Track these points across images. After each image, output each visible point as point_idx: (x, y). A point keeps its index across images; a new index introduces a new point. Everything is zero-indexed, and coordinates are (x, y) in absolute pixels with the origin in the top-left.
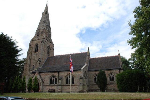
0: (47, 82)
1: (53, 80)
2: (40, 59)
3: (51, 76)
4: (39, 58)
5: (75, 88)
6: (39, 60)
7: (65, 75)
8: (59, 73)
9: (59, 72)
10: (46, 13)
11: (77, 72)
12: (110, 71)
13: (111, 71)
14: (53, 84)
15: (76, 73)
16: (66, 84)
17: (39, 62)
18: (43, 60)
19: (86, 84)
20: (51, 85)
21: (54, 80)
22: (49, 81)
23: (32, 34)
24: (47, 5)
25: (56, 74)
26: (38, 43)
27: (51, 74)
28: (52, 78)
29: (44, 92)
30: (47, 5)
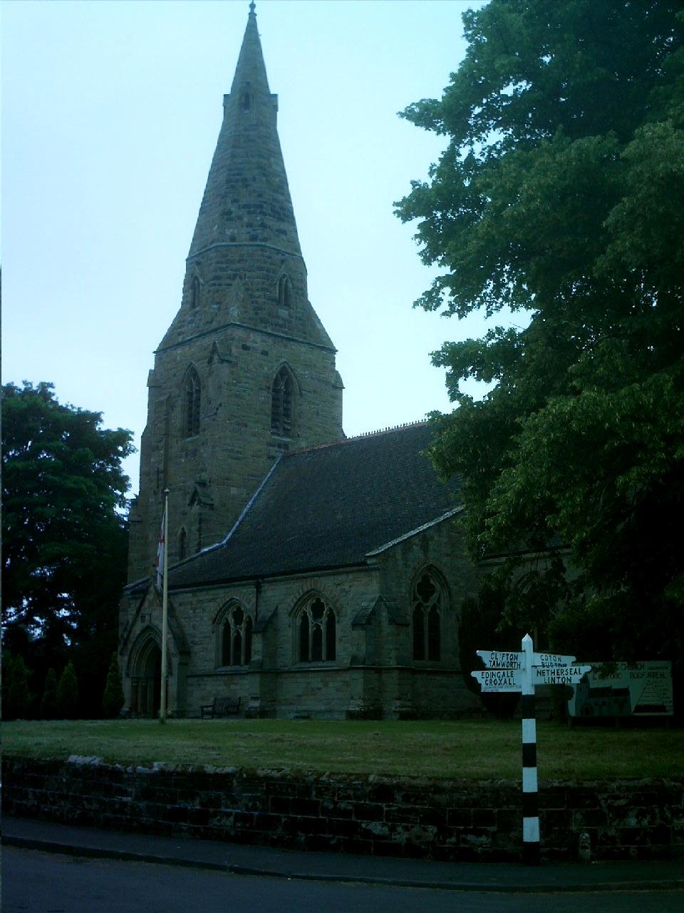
0: (207, 653)
1: (318, 632)
2: (203, 484)
3: (222, 612)
4: (204, 476)
5: (338, 690)
6: (195, 493)
7: (290, 601)
8: (259, 592)
9: (258, 581)
10: (250, 106)
11: (351, 576)
12: (221, 593)
13: (308, 585)
14: (237, 662)
15: (346, 587)
16: (297, 659)
17: (196, 508)
18: (234, 491)
19: (393, 663)
20: (229, 668)
21: (323, 627)
22: (214, 640)
23: (159, 300)
24: (252, 16)
25: (244, 596)
26: (201, 367)
27: (222, 595)
28: (310, 619)
29: (192, 715)
30: (252, 16)
